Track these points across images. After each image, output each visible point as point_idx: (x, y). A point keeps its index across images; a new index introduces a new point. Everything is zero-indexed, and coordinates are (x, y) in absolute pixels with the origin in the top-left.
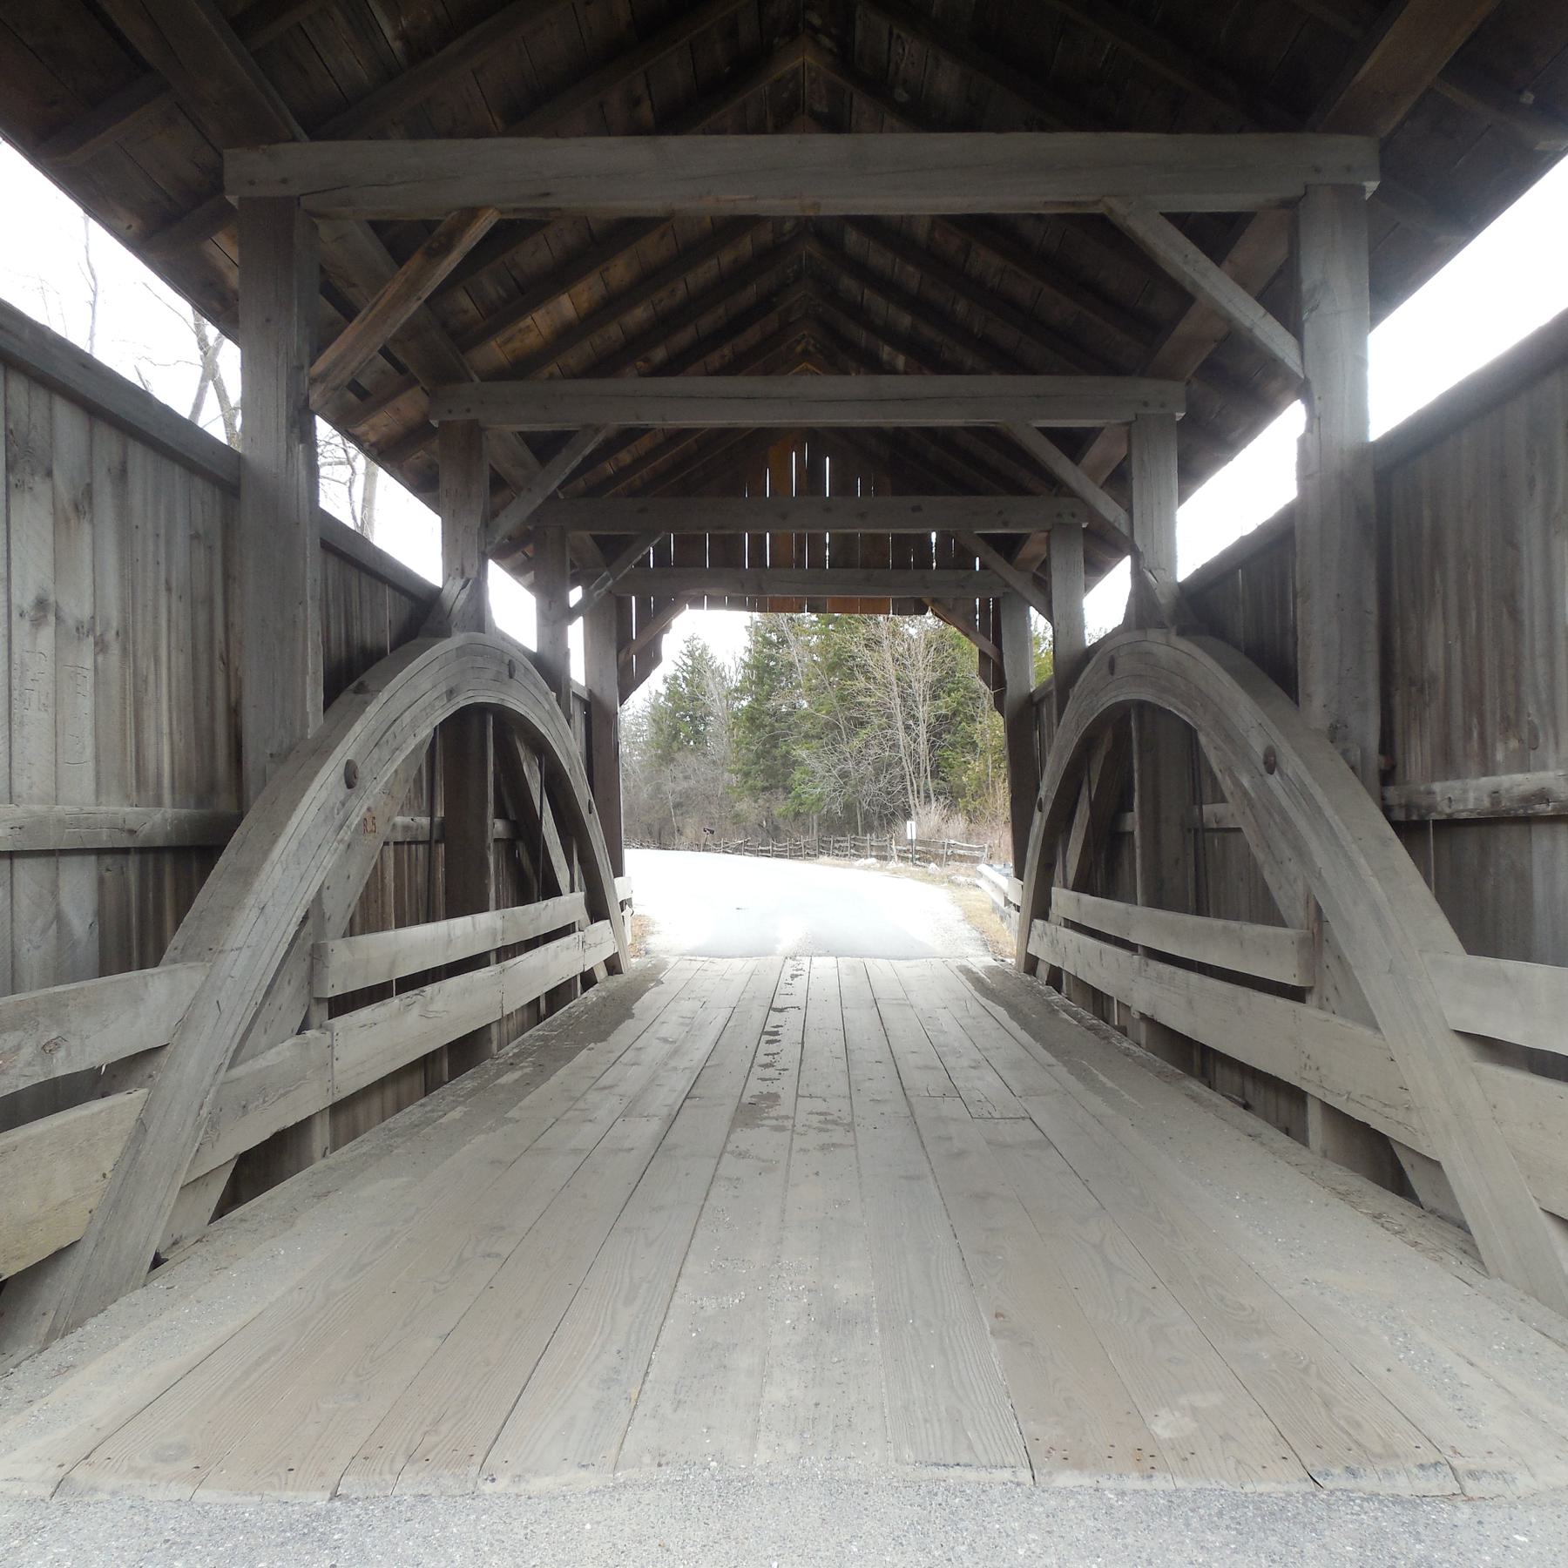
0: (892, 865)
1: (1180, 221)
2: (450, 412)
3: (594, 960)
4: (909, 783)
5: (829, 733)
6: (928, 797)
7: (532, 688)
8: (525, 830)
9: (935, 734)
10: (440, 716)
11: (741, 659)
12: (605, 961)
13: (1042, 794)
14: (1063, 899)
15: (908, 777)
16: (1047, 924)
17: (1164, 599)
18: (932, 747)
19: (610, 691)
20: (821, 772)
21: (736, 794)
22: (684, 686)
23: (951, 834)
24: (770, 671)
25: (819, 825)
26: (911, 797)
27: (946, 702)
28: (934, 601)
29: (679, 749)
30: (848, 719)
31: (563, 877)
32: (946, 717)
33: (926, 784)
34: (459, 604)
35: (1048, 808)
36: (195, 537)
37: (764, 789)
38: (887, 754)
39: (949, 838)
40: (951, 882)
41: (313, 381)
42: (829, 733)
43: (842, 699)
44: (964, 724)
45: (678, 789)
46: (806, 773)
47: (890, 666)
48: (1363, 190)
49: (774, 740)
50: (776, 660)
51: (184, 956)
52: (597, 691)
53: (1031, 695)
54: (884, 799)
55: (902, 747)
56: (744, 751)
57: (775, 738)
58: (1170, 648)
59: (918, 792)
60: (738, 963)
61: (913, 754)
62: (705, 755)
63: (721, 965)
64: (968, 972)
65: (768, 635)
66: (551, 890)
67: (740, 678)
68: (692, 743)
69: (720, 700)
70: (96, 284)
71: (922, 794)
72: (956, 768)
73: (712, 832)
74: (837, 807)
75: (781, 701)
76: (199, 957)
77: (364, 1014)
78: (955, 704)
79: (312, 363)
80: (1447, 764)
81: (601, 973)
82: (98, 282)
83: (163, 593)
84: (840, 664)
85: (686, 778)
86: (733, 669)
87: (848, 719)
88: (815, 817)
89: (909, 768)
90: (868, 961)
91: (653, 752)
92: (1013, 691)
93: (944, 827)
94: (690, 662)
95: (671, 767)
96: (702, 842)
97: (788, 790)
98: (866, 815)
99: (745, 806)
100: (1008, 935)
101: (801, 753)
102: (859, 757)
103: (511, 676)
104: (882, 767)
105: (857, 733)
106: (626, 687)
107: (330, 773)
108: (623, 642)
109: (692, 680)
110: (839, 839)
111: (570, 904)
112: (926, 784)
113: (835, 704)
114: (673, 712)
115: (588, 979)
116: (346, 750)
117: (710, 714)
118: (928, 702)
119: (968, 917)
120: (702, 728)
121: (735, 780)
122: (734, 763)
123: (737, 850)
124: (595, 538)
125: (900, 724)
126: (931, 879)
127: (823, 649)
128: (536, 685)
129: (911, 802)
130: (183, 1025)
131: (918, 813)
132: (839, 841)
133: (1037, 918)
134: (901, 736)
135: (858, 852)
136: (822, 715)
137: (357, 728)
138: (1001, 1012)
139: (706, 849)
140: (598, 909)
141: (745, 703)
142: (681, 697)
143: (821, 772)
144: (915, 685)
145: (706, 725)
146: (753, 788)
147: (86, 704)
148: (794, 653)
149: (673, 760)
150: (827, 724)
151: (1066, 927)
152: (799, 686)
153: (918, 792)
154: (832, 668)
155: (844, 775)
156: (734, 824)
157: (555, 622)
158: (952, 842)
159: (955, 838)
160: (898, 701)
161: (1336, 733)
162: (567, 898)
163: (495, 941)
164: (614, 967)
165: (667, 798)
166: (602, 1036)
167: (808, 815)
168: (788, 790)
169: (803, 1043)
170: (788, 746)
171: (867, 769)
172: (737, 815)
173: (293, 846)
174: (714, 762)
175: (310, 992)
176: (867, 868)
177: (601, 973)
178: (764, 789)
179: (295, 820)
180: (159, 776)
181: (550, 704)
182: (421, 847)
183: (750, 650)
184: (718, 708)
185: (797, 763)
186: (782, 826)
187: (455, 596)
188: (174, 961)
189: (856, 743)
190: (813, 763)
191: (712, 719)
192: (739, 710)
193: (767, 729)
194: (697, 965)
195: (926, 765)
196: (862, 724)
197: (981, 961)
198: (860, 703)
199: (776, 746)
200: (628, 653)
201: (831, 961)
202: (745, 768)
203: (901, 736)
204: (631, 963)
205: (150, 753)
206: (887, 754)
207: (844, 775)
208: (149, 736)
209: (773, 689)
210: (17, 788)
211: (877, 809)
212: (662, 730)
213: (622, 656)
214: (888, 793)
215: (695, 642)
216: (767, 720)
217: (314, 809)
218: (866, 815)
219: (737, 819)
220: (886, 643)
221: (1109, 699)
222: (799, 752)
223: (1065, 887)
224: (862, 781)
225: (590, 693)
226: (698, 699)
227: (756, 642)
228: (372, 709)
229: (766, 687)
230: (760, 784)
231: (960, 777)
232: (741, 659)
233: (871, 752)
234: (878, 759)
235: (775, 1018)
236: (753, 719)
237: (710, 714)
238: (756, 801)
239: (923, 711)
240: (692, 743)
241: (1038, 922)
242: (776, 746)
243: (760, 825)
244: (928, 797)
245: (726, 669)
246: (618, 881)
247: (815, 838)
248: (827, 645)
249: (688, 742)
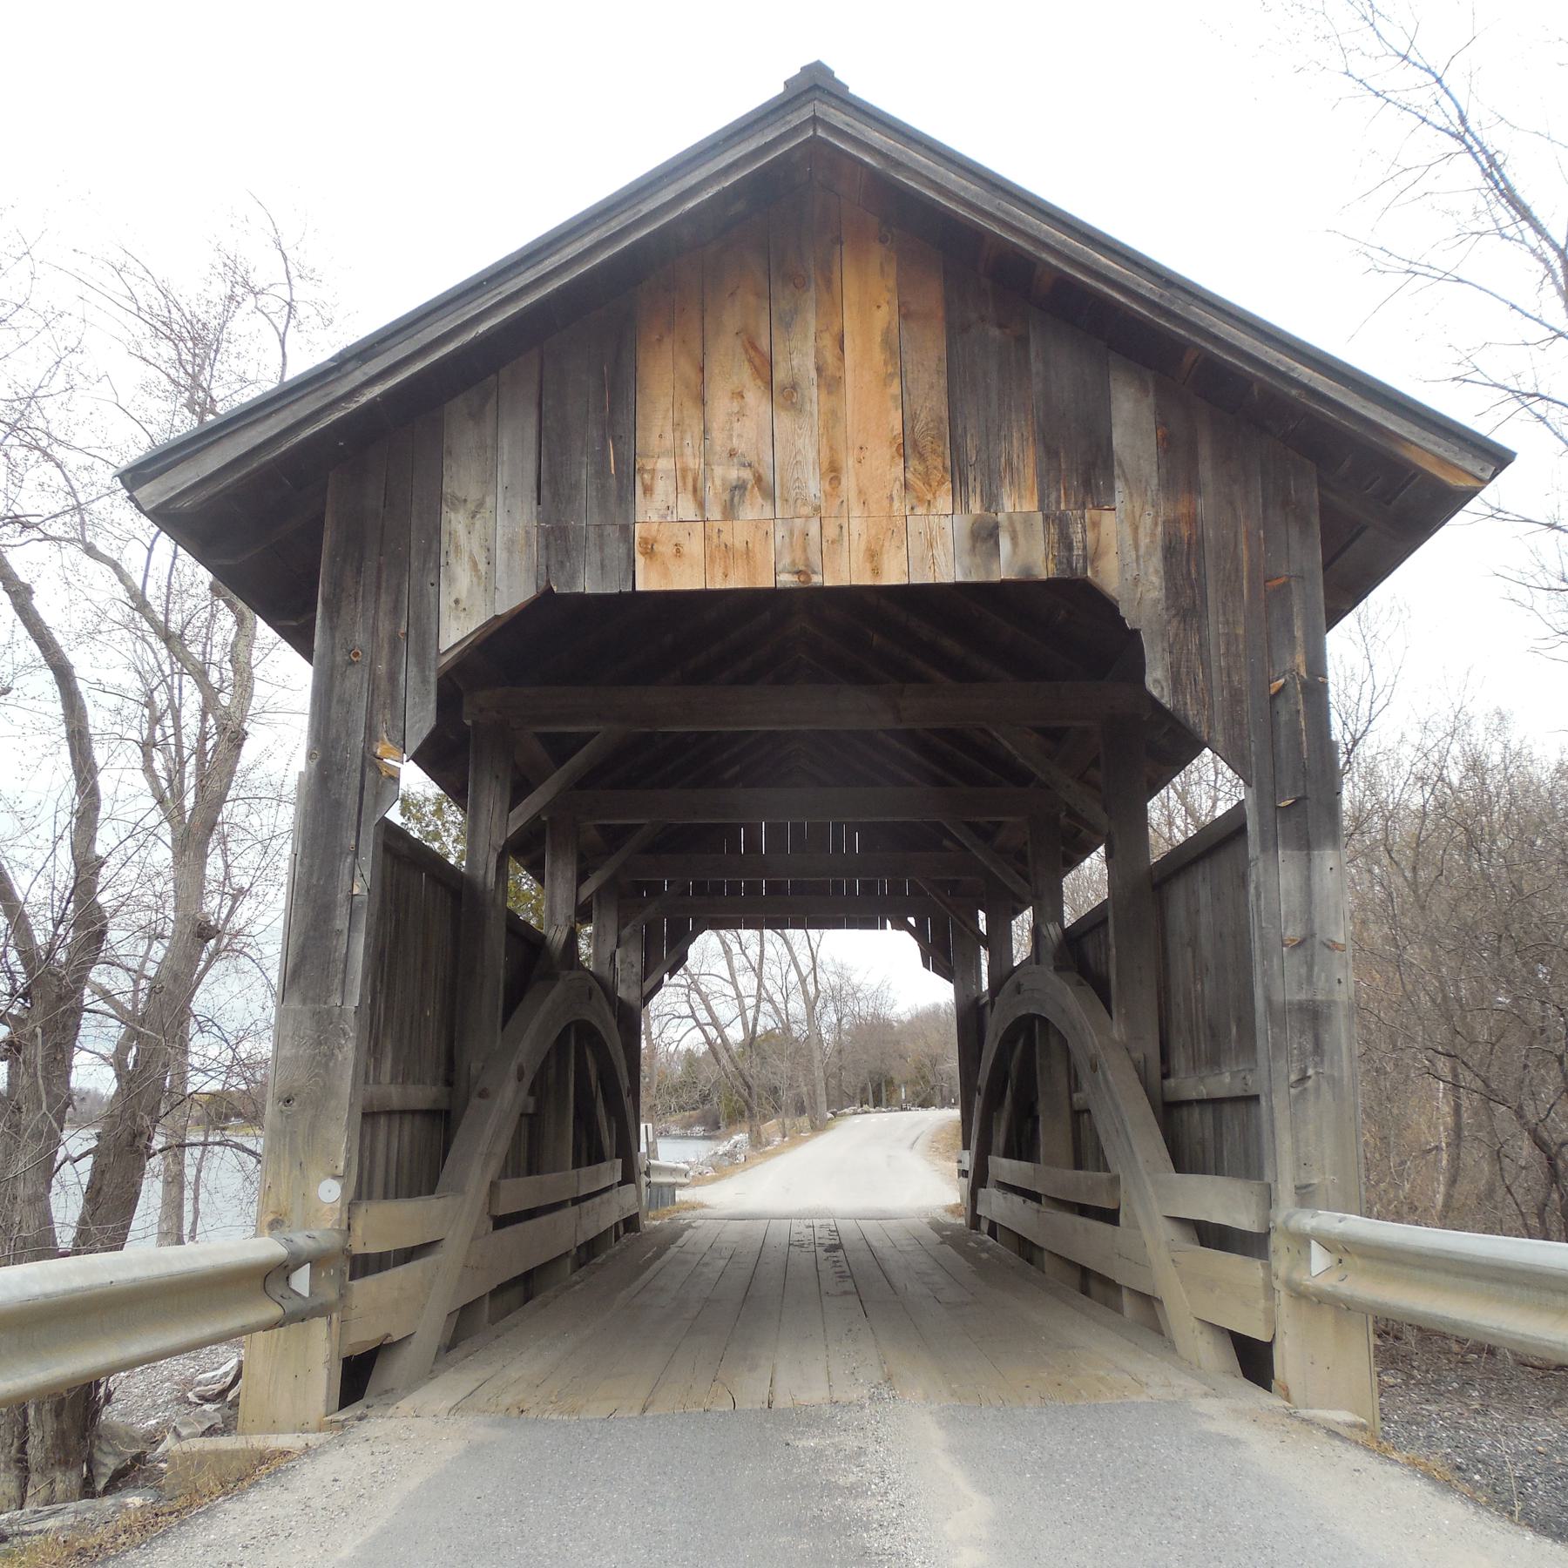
141: (452, 737)
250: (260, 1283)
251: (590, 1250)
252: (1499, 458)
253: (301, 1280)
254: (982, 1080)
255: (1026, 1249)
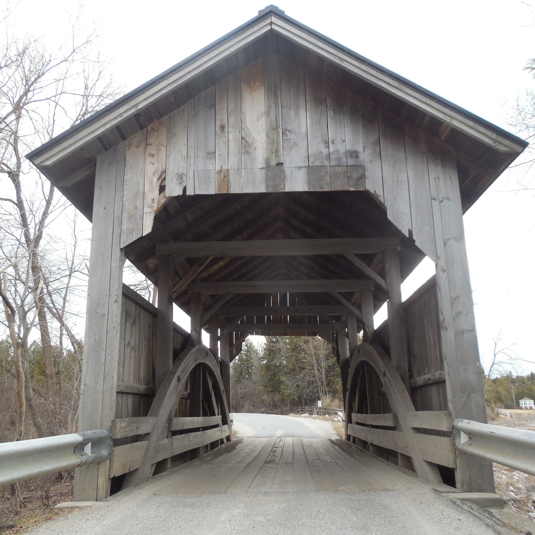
0: (314, 416)
1: (357, 255)
2: (193, 290)
3: (224, 436)
4: (319, 389)
5: (292, 372)
6: (326, 393)
7: (211, 359)
8: (207, 398)
9: (328, 372)
10: (194, 366)
11: (263, 347)
12: (226, 437)
13: (348, 387)
14: (354, 416)
15: (319, 387)
16: (351, 424)
17: (370, 335)
18: (327, 376)
19: (227, 359)
20: (290, 385)
21: (262, 393)
22: (244, 356)
23: (334, 405)
24: (273, 351)
25: (290, 403)
26: (320, 393)
27: (331, 361)
28: (319, 332)
29: (242, 378)
30: (299, 367)
31: (216, 411)
32: (331, 366)
33: (325, 389)
34: (196, 337)
35: (349, 390)
36: (149, 327)
37: (272, 391)
38: (312, 379)
39: (333, 407)
40: (332, 420)
41: (173, 292)
42: (292, 372)
43: (297, 360)
44: (337, 368)
45: (242, 392)
46: (285, 385)
47: (312, 349)
48: (397, 249)
49: (274, 375)
50: (275, 347)
51: (151, 415)
52: (224, 359)
53: (347, 359)
54: (311, 394)
55: (317, 376)
56: (265, 379)
57: (275, 374)
58: (369, 347)
59: (323, 392)
60: (264, 439)
61: (320, 379)
62: (251, 380)
63: (259, 439)
64: (332, 442)
65: (272, 339)
66: (213, 414)
67: (263, 354)
68: (247, 376)
69: (256, 361)
70: (76, 240)
71: (324, 392)
72: (335, 383)
73: (254, 406)
74: (296, 397)
75: (277, 361)
76: (154, 416)
77: (178, 437)
78: (334, 362)
79: (173, 289)
80: (419, 375)
81: (225, 441)
82: (77, 239)
83: (144, 339)
84: (295, 349)
85: (245, 388)
86: (261, 350)
87: (299, 367)
88: (288, 401)
89: (319, 383)
90: (302, 438)
91: (234, 379)
92: (342, 358)
93: (331, 403)
94: (246, 348)
95: (240, 384)
96: (251, 410)
97: (279, 391)
98: (306, 400)
99: (265, 397)
100: (343, 431)
101: (283, 379)
102: (303, 380)
103: (207, 356)
104: (310, 383)
105: (302, 372)
106: (232, 358)
107: (175, 378)
108: (231, 345)
109: (247, 354)
110: (297, 408)
111: (217, 419)
112: (325, 389)
113: (295, 362)
114: (240, 365)
115: (222, 441)
116: (178, 374)
117: (253, 366)
118: (325, 361)
119: (335, 429)
120: (250, 371)
121: (262, 388)
122: (262, 383)
123: (262, 413)
124: (225, 317)
125: (316, 369)
126: (326, 420)
127: (290, 345)
128: (212, 357)
129: (320, 395)
130: (153, 429)
131: (322, 399)
132: (297, 409)
133: (349, 423)
134: (316, 372)
135: (303, 412)
136: (290, 366)
137: (180, 368)
138: (337, 447)
139: (252, 412)
140: (225, 421)
141: (265, 362)
142: (243, 360)
143: (290, 385)
144: (321, 355)
145: (252, 370)
146: (268, 391)
147: (133, 363)
148: (281, 345)
149: (241, 382)
150: (292, 369)
151: (356, 424)
152: (283, 356)
153: (323, 392)
154: (293, 350)
155: (298, 386)
156: (261, 404)
157: (214, 340)
158: (334, 408)
159: (335, 407)
160: (315, 361)
161: (398, 368)
162: (217, 416)
163: (202, 424)
164: (228, 439)
165: (239, 395)
166: (230, 452)
167: (286, 400)
168: (279, 391)
169: (282, 453)
170: (279, 376)
171: (305, 384)
172: (263, 401)
173: (169, 394)
174: (255, 382)
175: (169, 429)
176: (306, 417)
177: (225, 441)
178: (272, 391)
179: (170, 388)
180: (142, 378)
181: (215, 363)
182: (184, 400)
183: (266, 345)
184: (255, 364)
185: (282, 382)
186: (278, 404)
187: (195, 336)
188: (150, 416)
189: (301, 375)
190: (287, 382)
191: (254, 367)
192: (263, 364)
193: (272, 371)
194: (253, 439)
195: (325, 382)
196: (303, 369)
197: (335, 437)
198: (302, 362)
199: (275, 377)
200: (233, 348)
201: (292, 438)
202: (265, 385)
203: (316, 372)
204: (233, 439)
205: (141, 374)
206: (312, 379)
207: (298, 386)
208: (141, 370)
209: (274, 357)
210: (124, 380)
211: (309, 398)
212: (237, 372)
213: (231, 349)
214: (313, 392)
215: (248, 341)
216: (272, 368)
217: (173, 386)
218: (306, 400)
219: (263, 402)
220: (310, 342)
221: (358, 361)
222: (283, 379)
223: (355, 413)
224: (304, 388)
225: (222, 360)
226: (249, 361)
227: (268, 342)
228: (182, 364)
229: (272, 357)
230: (270, 390)
231: (336, 386)
232: (263, 347)
233: (307, 378)
234: (309, 381)
235: (274, 449)
236: (268, 367)
237: (253, 366)
238: (269, 396)
239: (323, 364)
240: (247, 376)
241: (349, 424)
242: (275, 377)
243: (270, 404)
244: (326, 393)
245: (258, 350)
246: (230, 414)
247: (289, 408)
248: (292, 343)
249: (246, 376)
250: (73, 450)
251: (214, 445)
252: (524, 145)
253: (88, 449)
254: (349, 386)
255: (364, 444)
